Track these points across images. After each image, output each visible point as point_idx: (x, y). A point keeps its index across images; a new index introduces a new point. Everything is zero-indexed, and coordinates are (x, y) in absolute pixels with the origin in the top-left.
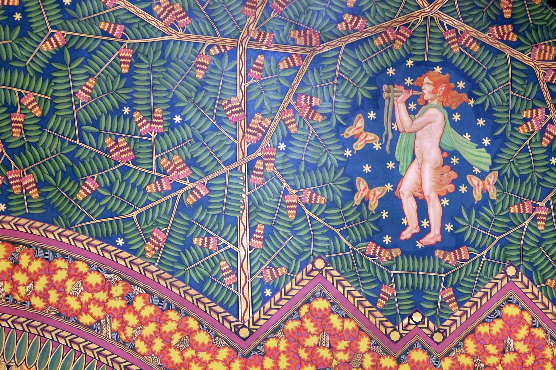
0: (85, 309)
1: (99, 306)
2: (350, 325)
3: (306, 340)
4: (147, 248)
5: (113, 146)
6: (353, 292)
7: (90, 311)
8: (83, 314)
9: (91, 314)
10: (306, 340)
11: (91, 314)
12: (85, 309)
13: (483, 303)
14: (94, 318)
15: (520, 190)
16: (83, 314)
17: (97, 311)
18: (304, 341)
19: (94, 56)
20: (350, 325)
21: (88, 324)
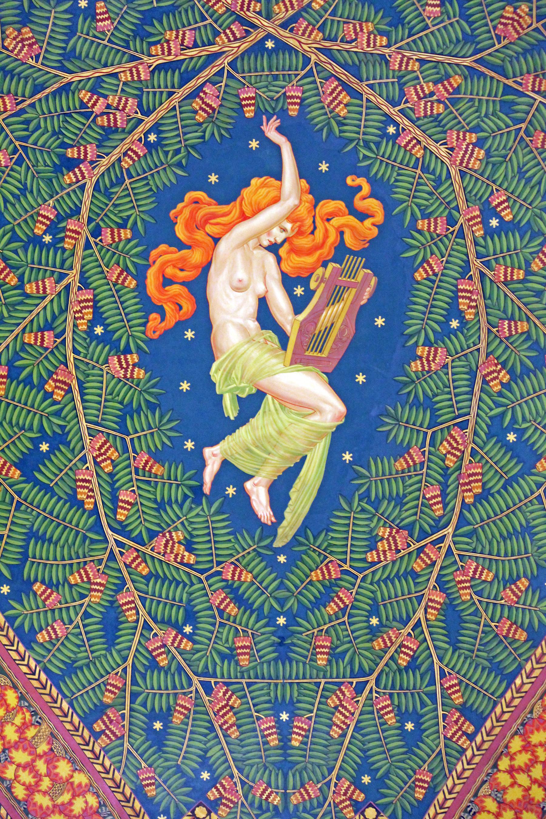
0: (527, 747)
1: (526, 765)
2: (80, 778)
3: (73, 808)
4: (111, 97)
5: (422, 363)
6: (28, 672)
7: (523, 753)
8: (523, 743)
9: (520, 752)
10: (73, 808)
11: (520, 752)
12: (527, 747)
13: (95, 765)
14: (515, 754)
15: (12, 545)
16: (523, 743)
17: (522, 759)
18: (72, 811)
19: (453, 337)
20: (80, 778)
21: (510, 745)
